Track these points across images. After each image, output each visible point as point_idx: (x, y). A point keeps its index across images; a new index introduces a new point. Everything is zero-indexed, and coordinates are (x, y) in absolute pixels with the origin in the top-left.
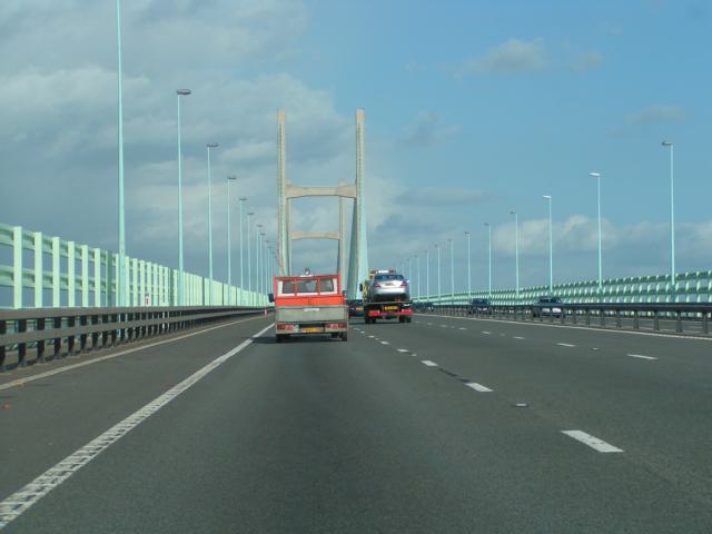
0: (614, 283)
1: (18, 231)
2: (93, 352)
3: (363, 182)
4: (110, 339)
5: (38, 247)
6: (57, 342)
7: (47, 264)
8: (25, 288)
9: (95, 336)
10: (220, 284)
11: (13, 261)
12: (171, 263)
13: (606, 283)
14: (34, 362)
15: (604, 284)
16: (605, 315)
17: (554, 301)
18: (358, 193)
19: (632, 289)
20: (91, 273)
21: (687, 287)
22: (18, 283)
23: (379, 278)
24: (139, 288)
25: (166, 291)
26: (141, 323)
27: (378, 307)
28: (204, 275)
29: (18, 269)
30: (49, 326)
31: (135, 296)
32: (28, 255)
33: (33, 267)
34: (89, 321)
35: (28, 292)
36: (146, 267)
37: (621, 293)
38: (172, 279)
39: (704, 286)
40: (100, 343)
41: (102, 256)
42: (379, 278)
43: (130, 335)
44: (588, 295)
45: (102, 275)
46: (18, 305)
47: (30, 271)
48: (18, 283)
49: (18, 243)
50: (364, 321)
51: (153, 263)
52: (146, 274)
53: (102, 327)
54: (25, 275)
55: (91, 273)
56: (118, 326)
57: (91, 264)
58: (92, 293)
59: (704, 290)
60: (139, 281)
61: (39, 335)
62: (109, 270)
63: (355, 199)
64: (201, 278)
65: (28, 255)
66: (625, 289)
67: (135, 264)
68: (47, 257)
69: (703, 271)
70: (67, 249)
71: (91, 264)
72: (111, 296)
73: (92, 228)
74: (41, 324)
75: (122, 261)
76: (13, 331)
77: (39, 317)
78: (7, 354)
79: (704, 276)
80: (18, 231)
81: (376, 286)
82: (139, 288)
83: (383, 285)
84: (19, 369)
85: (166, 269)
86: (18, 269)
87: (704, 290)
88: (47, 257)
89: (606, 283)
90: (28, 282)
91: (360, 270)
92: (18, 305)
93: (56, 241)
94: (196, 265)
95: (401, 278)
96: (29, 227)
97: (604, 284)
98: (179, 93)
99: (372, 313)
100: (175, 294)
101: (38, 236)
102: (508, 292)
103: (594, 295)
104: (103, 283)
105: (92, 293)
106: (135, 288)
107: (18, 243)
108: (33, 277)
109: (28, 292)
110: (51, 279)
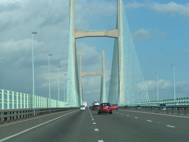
0: (179, 99)
1: (3, 90)
2: (13, 121)
3: (104, 71)
4: (48, 113)
5: (13, 95)
6: (17, 116)
7: (19, 99)
8: (5, 104)
9: (29, 115)
10: (56, 101)
11: (1, 97)
12: (30, 92)
13: (177, 99)
14: (9, 121)
15: (176, 100)
16: (152, 109)
17: (164, 105)
18: (103, 74)
19: (170, 102)
20: (26, 100)
21: (181, 101)
22: (3, 103)
23: (95, 102)
24: (41, 103)
25: (46, 104)
26: (52, 110)
27: (94, 107)
28: (57, 100)
29: (3, 99)
30: (15, 113)
31: (40, 105)
32: (6, 96)
33: (7, 99)
34: (12, 113)
35: (6, 105)
36: (40, 98)
37: (182, 102)
38: (48, 101)
39: (187, 101)
40: (36, 115)
41: (29, 96)
42: (95, 102)
43: (31, 116)
44: (154, 104)
45: (29, 100)
46: (3, 108)
47: (16, 101)
48: (3, 103)
49: (3, 93)
50: (171, 113)
51: (42, 97)
52: (40, 100)
53: (28, 113)
54: (10, 101)
55: (26, 100)
56: (50, 110)
57: (26, 98)
58: (26, 105)
59: (187, 102)
60: (40, 102)
61: (17, 115)
62: (31, 99)
63: (102, 76)
64: (56, 101)
65: (6, 96)
66: (183, 101)
67: (45, 99)
68: (19, 97)
69: (187, 97)
70: (27, 96)
71: (26, 98)
72: (31, 105)
73: (23, 88)
74: (17, 112)
75: (34, 97)
76: (3, 114)
77: (5, 111)
78: (1, 120)
79: (187, 98)
80: (3, 90)
81: (94, 104)
82: (41, 103)
83: (95, 103)
84: (10, 122)
85: (46, 98)
86: (3, 99)
87: (187, 102)
88: (19, 97)
89: (177, 99)
90: (19, 103)
91: (104, 97)
92: (3, 108)
93: (21, 94)
94: (55, 97)
95: (98, 102)
96: (6, 89)
97: (176, 100)
98: (49, 55)
99: (94, 108)
100: (49, 105)
101: (17, 93)
102: (155, 101)
103: (173, 103)
104: (29, 102)
105: (26, 105)
106: (45, 104)
107: (3, 93)
108: (12, 102)
109: (6, 105)
110: (16, 102)
